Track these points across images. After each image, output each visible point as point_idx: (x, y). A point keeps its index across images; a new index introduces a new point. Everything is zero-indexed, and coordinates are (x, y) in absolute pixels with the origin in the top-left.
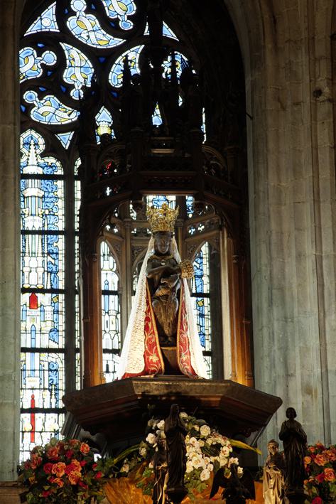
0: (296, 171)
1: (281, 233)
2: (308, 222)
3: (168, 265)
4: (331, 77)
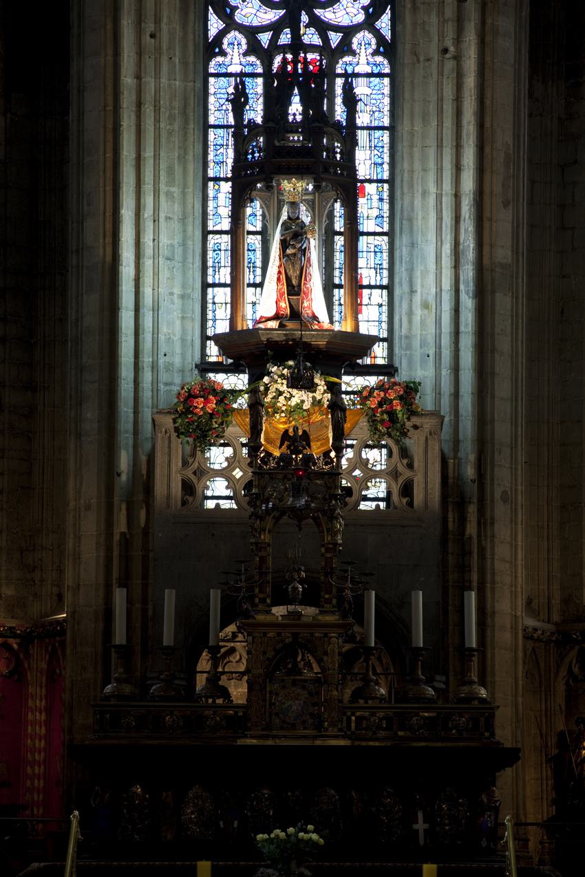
0: (425, 119)
1: (412, 171)
2: (432, 165)
3: (297, 229)
4: (456, 37)
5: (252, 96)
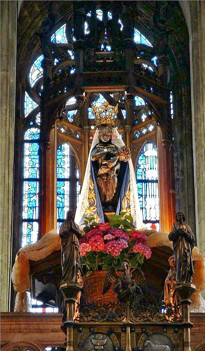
5: (60, 157)
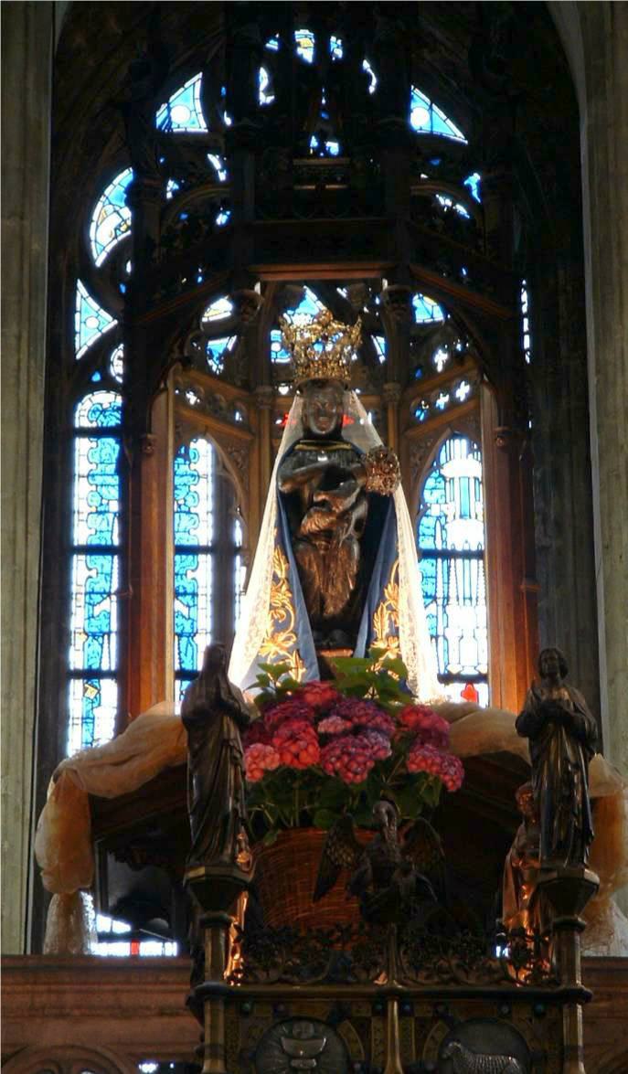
5: (185, 479)
